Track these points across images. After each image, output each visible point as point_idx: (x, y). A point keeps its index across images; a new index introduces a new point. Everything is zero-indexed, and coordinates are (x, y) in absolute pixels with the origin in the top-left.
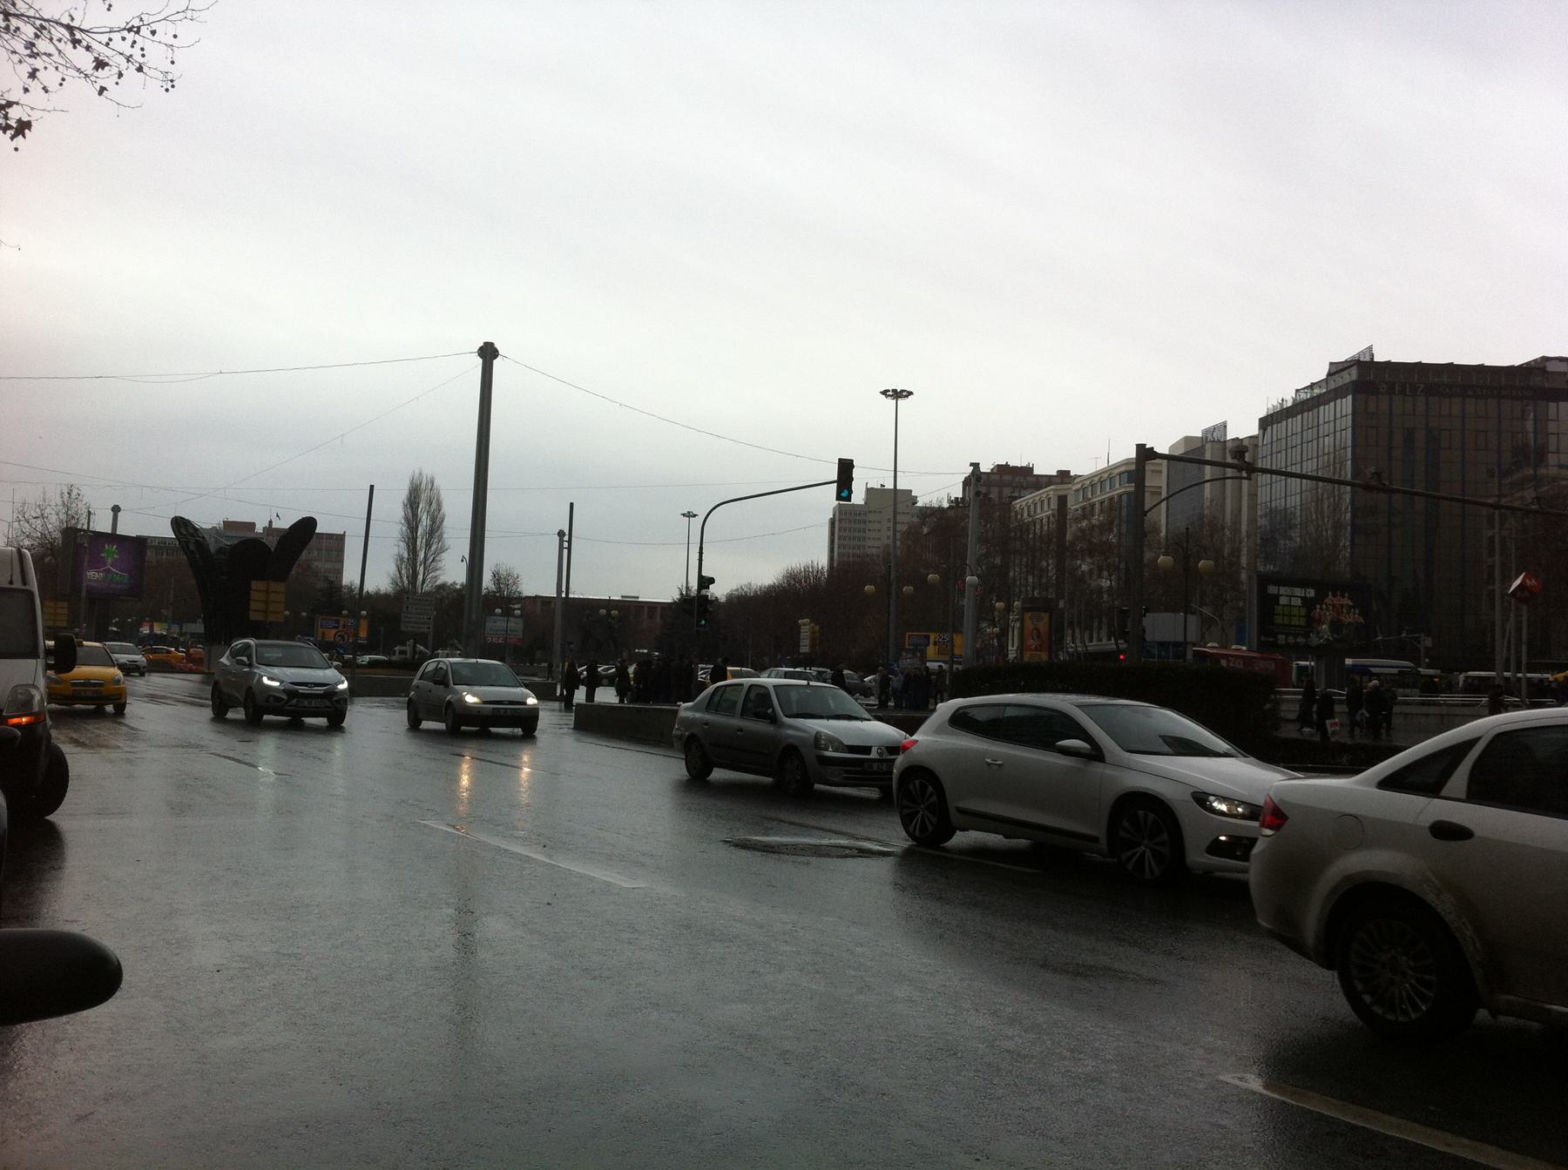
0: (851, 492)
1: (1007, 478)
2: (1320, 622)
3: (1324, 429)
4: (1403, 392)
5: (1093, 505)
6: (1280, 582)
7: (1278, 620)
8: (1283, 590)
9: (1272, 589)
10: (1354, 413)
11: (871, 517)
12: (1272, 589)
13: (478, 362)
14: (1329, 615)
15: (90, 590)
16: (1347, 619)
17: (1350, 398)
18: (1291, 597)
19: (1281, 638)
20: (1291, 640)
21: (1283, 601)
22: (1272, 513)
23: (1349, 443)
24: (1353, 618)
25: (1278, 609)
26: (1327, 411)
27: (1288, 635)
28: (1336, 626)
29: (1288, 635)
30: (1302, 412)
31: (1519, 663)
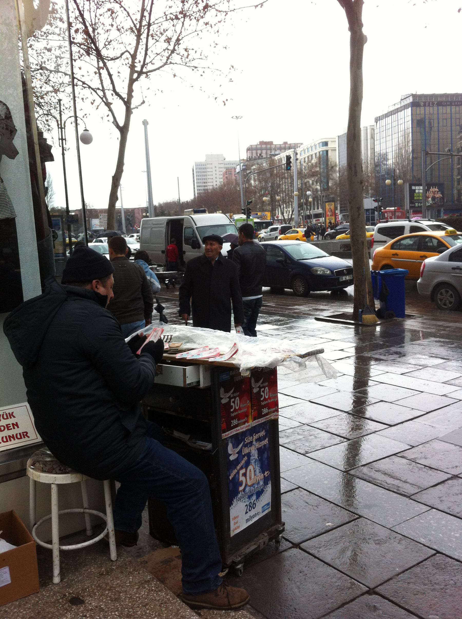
0: (291, 167)
1: (264, 146)
2: (428, 198)
3: (401, 121)
4: (429, 105)
5: (312, 155)
6: (415, 185)
7: (415, 198)
8: (417, 188)
9: (413, 188)
10: (412, 115)
11: (208, 166)
12: (413, 188)
13: (143, 126)
14: (431, 195)
15: (368, 241)
16: (437, 196)
17: (410, 108)
18: (419, 190)
19: (417, 204)
20: (420, 205)
21: (417, 191)
22: (380, 154)
23: (410, 126)
24: (439, 195)
25: (415, 195)
26: (401, 114)
27: (418, 203)
28: (434, 198)
29: (418, 203)
30: (391, 115)
31: (199, 179)
